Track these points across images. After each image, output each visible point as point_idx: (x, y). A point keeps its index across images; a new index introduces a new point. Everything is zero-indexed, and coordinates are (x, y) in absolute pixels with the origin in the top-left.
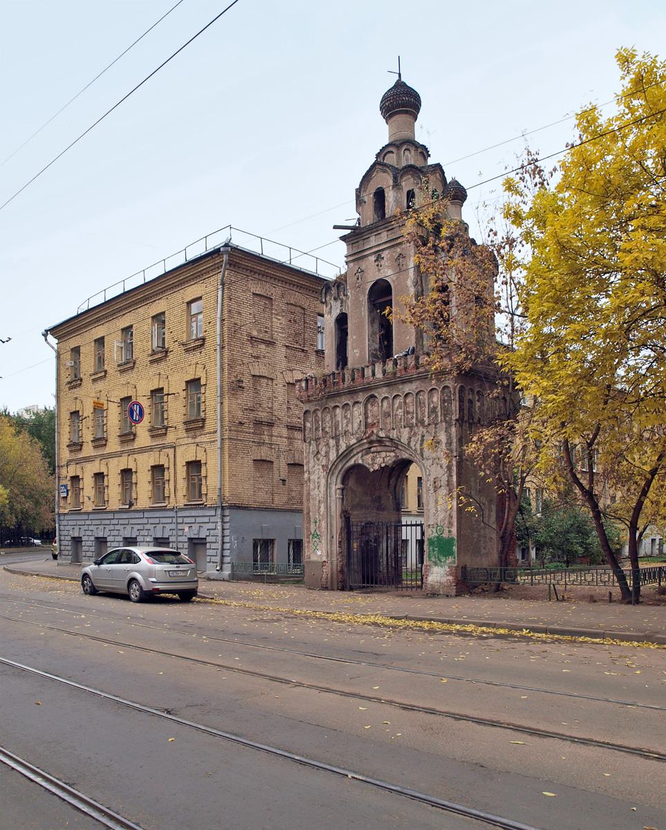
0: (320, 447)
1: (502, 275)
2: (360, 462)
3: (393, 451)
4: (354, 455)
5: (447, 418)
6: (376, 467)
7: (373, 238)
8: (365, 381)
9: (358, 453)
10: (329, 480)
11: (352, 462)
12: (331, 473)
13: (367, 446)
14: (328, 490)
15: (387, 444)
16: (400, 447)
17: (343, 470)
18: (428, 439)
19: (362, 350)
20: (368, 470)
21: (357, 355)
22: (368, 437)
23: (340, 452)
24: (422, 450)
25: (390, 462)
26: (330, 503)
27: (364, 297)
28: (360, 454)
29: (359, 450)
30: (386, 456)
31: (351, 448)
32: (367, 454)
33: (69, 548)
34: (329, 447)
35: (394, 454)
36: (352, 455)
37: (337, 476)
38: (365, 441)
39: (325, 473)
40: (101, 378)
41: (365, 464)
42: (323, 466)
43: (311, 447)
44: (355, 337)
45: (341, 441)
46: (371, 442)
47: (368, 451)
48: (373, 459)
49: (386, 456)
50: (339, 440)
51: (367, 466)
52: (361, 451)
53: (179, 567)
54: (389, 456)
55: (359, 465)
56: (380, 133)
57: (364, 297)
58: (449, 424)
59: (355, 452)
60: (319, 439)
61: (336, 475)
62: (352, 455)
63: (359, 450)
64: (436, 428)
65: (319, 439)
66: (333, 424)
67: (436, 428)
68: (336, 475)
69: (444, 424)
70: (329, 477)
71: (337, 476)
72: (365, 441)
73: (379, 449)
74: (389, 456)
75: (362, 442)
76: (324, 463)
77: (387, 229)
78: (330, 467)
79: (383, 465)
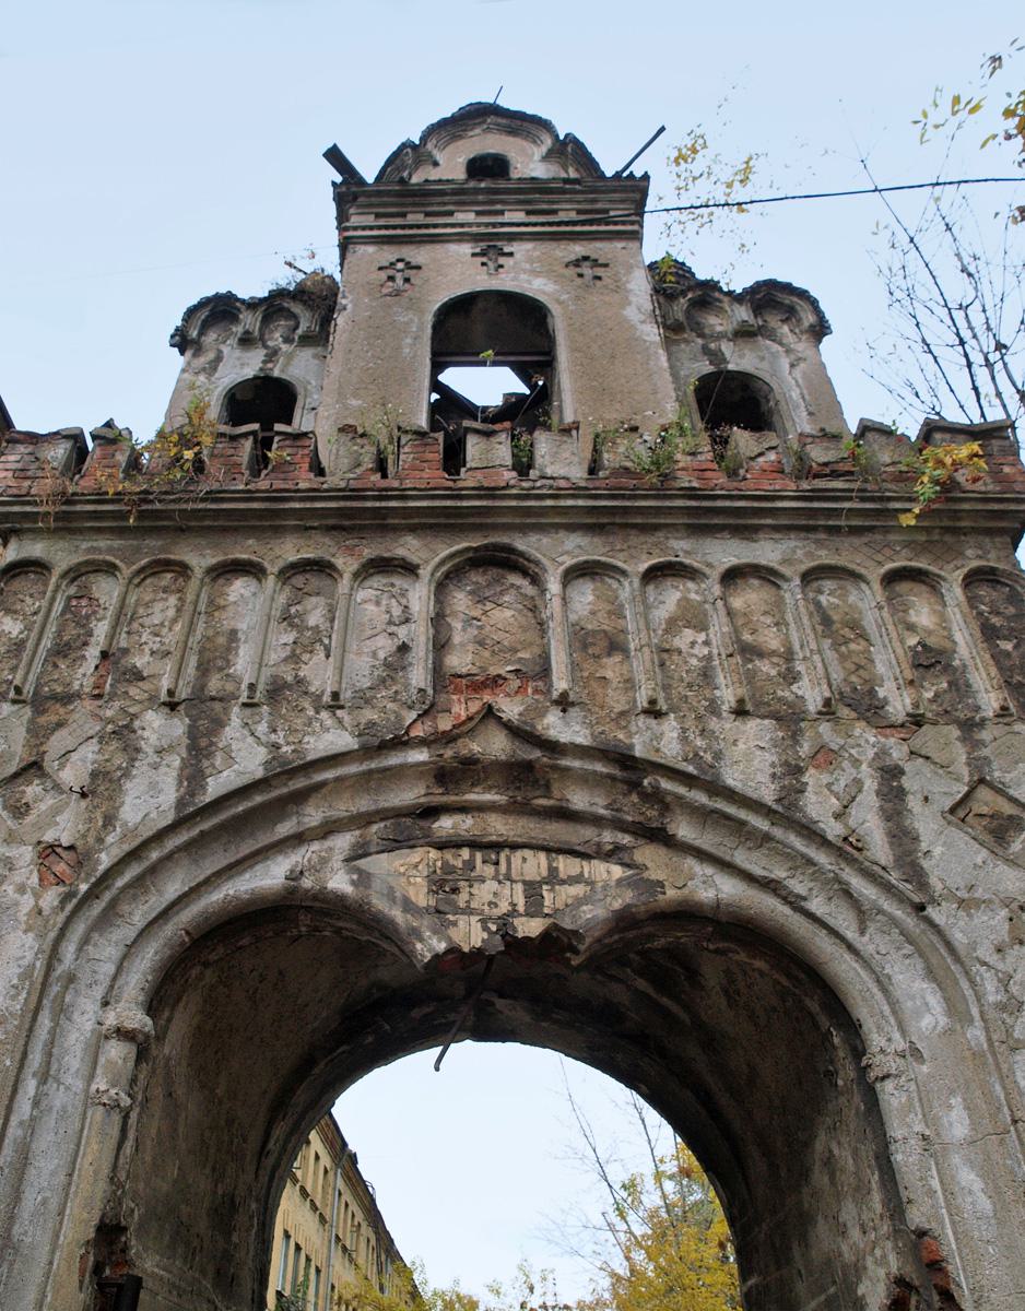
2: (339, 882)
3: (612, 854)
4: (299, 839)
6: (471, 934)
8: (467, 479)
9: (328, 829)
10: (69, 950)
11: (271, 876)
12: (97, 907)
13: (409, 795)
14: (45, 1021)
15: (579, 800)
16: (684, 830)
17: (187, 915)
22: (449, 738)
23: (215, 787)
24: (902, 837)
26: (32, 1125)
28: (343, 842)
29: (344, 806)
30: (553, 878)
31: (299, 783)
32: (395, 844)
34: (133, 751)
35: (617, 871)
36: (285, 829)
37: (131, 949)
38: (420, 756)
39: (50, 898)
41: (379, 904)
42: (49, 851)
46: (467, 771)
47: (409, 827)
48: (444, 884)
49: (553, 878)
51: (398, 915)
52: (363, 820)
53: (594, 201)
54: (577, 879)
55: (328, 907)
59: (313, 815)
60: (67, 698)
61: (124, 933)
62: (285, 829)
63: (344, 806)
65: (67, 698)
66: (193, 641)
68: (124, 933)
70: (79, 928)
71: (131, 949)
72: (420, 756)
73: (499, 826)
74: (577, 879)
75: (394, 759)
76: (65, 829)
77: (530, 207)
78: (105, 860)
79: (530, 928)
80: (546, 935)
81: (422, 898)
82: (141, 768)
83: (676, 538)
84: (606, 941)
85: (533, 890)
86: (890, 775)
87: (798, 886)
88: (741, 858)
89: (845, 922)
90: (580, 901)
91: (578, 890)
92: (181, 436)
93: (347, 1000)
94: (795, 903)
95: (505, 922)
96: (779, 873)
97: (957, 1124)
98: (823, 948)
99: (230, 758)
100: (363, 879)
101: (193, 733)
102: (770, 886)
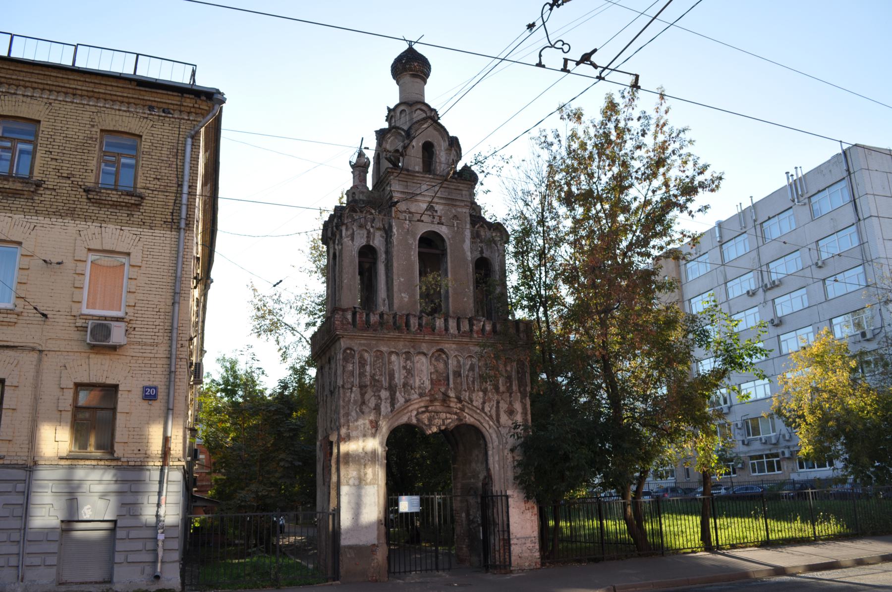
0: (367, 396)
1: (26, 262)
2: (414, 421)
5: (522, 389)
6: (435, 429)
7: (11, 183)
18: (504, 406)
19: (412, 296)
20: (422, 432)
21: (406, 300)
25: (452, 425)
27: (415, 241)
33: (777, 536)
40: (128, 206)
43: (353, 395)
44: (402, 280)
45: (398, 394)
49: (447, 418)
50: (395, 393)
56: (392, 96)
57: (415, 241)
58: (523, 396)
60: (366, 386)
64: (510, 396)
67: (510, 396)
69: (519, 394)
74: (449, 419)
79: (443, 428)
80: (445, 429)
81: (426, 422)
82: (383, 403)
83: (507, 542)
84: (367, 274)
85: (443, 420)
86: (498, 403)
87: (482, 421)
88: (475, 415)
89: (487, 427)
90: (450, 423)
91: (450, 420)
92: (382, 326)
93: (309, 344)
94: (481, 423)
95: (439, 427)
96: (480, 419)
97: (497, 458)
98: (483, 430)
99: (398, 401)
100: (418, 420)
101: (391, 395)
102: (478, 421)
